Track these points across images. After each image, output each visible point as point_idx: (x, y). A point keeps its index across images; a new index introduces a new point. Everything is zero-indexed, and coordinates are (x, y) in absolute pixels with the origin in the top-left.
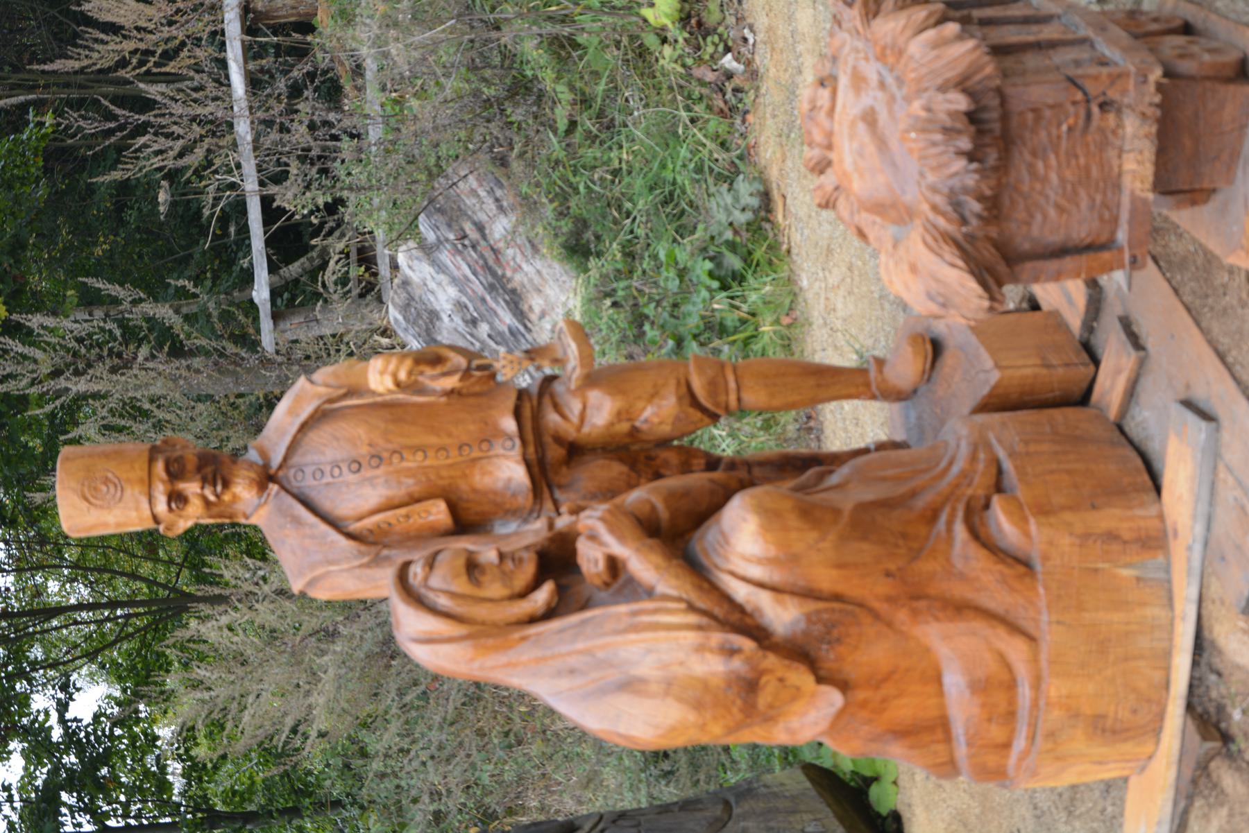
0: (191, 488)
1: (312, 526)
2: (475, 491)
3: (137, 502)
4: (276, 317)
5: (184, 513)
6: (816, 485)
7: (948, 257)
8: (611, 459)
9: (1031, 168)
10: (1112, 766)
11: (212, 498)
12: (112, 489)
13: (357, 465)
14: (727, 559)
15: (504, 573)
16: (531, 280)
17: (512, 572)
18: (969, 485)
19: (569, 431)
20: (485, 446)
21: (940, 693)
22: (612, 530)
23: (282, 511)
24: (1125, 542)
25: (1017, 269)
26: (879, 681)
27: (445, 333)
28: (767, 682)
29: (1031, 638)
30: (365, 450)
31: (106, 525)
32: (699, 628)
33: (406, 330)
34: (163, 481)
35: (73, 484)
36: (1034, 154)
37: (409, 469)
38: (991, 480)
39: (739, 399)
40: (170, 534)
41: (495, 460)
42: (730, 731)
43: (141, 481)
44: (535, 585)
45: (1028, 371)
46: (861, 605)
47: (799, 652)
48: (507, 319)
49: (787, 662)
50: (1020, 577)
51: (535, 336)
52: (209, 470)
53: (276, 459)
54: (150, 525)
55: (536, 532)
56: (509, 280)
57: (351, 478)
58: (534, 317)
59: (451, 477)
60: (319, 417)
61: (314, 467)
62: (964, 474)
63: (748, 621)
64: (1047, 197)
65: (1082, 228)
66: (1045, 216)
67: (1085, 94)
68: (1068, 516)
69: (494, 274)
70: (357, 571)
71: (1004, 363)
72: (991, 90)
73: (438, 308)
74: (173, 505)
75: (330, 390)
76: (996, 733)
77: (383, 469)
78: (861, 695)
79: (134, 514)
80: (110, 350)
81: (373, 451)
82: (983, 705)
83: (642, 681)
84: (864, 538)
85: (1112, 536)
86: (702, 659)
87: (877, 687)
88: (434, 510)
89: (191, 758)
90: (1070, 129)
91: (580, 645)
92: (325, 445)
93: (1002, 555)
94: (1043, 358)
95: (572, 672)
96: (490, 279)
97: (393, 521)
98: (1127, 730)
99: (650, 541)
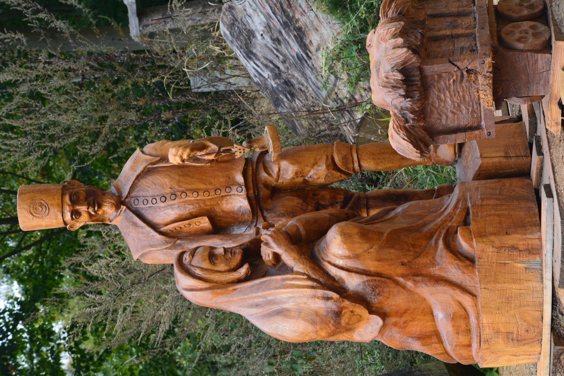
0: (83, 209)
1: (142, 228)
2: (223, 211)
3: (56, 215)
4: (141, 14)
5: (79, 220)
6: (382, 217)
7: (402, 135)
8: (294, 196)
9: (439, 98)
10: (522, 357)
11: (93, 213)
12: (44, 209)
13: (164, 198)
14: (327, 256)
15: (226, 259)
16: (312, 22)
17: (230, 258)
18: (450, 221)
19: (272, 180)
20: (228, 190)
21: (434, 320)
22: (275, 240)
23: (127, 219)
24: (520, 251)
25: (436, 138)
26: (402, 313)
27: (258, 47)
28: (346, 312)
29: (473, 295)
30: (168, 190)
31: (41, 226)
32: (313, 287)
33: (232, 42)
34: (69, 205)
35: (25, 206)
36: (440, 92)
37: (190, 201)
38: (461, 219)
39: (360, 166)
40: (72, 229)
41: (233, 197)
42: (330, 335)
43: (58, 205)
44: (240, 266)
45: (496, 160)
46: (390, 278)
47: (359, 299)
48: (296, 48)
49: (353, 304)
50: (467, 267)
51: (314, 62)
52: (91, 199)
53: (125, 193)
54: (62, 225)
55: (250, 235)
56: (297, 21)
57: (162, 205)
58: (313, 49)
59: (211, 205)
60: (147, 172)
61: (144, 198)
62: (450, 216)
63: (336, 284)
64: (447, 109)
65: (464, 120)
66: (447, 117)
67: (458, 67)
68: (493, 238)
69: (287, 16)
70: (165, 251)
71: (485, 155)
72: (416, 67)
73: (254, 28)
74: (74, 217)
75: (152, 158)
76: (463, 339)
77: (177, 201)
78: (393, 320)
79: (55, 221)
80: (19, 52)
81: (172, 191)
82: (453, 326)
83: (288, 310)
84: (392, 247)
85: (514, 248)
86: (316, 302)
87: (401, 316)
88: (203, 221)
89: (81, 352)
90: (454, 81)
91: (260, 294)
92: (149, 187)
93: (459, 256)
94: (506, 153)
95: (257, 306)
96: (284, 19)
97: (183, 227)
98: (525, 340)
99: (292, 247)
